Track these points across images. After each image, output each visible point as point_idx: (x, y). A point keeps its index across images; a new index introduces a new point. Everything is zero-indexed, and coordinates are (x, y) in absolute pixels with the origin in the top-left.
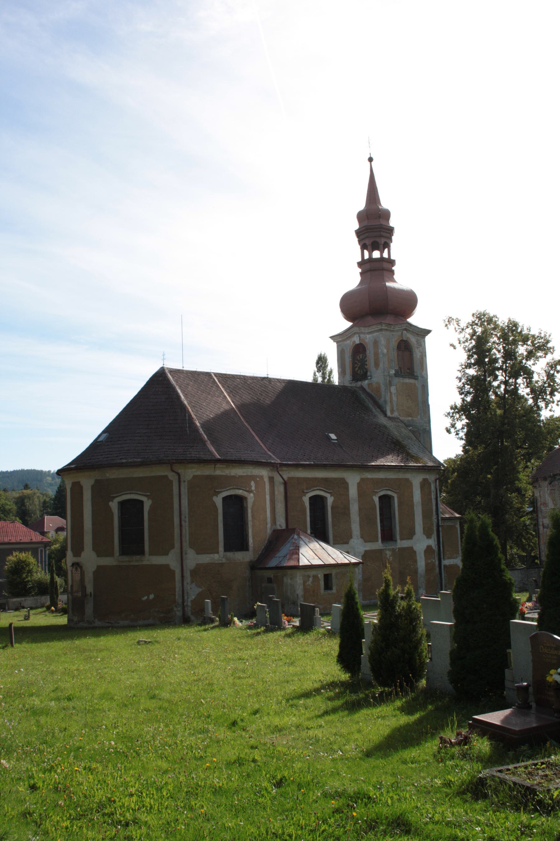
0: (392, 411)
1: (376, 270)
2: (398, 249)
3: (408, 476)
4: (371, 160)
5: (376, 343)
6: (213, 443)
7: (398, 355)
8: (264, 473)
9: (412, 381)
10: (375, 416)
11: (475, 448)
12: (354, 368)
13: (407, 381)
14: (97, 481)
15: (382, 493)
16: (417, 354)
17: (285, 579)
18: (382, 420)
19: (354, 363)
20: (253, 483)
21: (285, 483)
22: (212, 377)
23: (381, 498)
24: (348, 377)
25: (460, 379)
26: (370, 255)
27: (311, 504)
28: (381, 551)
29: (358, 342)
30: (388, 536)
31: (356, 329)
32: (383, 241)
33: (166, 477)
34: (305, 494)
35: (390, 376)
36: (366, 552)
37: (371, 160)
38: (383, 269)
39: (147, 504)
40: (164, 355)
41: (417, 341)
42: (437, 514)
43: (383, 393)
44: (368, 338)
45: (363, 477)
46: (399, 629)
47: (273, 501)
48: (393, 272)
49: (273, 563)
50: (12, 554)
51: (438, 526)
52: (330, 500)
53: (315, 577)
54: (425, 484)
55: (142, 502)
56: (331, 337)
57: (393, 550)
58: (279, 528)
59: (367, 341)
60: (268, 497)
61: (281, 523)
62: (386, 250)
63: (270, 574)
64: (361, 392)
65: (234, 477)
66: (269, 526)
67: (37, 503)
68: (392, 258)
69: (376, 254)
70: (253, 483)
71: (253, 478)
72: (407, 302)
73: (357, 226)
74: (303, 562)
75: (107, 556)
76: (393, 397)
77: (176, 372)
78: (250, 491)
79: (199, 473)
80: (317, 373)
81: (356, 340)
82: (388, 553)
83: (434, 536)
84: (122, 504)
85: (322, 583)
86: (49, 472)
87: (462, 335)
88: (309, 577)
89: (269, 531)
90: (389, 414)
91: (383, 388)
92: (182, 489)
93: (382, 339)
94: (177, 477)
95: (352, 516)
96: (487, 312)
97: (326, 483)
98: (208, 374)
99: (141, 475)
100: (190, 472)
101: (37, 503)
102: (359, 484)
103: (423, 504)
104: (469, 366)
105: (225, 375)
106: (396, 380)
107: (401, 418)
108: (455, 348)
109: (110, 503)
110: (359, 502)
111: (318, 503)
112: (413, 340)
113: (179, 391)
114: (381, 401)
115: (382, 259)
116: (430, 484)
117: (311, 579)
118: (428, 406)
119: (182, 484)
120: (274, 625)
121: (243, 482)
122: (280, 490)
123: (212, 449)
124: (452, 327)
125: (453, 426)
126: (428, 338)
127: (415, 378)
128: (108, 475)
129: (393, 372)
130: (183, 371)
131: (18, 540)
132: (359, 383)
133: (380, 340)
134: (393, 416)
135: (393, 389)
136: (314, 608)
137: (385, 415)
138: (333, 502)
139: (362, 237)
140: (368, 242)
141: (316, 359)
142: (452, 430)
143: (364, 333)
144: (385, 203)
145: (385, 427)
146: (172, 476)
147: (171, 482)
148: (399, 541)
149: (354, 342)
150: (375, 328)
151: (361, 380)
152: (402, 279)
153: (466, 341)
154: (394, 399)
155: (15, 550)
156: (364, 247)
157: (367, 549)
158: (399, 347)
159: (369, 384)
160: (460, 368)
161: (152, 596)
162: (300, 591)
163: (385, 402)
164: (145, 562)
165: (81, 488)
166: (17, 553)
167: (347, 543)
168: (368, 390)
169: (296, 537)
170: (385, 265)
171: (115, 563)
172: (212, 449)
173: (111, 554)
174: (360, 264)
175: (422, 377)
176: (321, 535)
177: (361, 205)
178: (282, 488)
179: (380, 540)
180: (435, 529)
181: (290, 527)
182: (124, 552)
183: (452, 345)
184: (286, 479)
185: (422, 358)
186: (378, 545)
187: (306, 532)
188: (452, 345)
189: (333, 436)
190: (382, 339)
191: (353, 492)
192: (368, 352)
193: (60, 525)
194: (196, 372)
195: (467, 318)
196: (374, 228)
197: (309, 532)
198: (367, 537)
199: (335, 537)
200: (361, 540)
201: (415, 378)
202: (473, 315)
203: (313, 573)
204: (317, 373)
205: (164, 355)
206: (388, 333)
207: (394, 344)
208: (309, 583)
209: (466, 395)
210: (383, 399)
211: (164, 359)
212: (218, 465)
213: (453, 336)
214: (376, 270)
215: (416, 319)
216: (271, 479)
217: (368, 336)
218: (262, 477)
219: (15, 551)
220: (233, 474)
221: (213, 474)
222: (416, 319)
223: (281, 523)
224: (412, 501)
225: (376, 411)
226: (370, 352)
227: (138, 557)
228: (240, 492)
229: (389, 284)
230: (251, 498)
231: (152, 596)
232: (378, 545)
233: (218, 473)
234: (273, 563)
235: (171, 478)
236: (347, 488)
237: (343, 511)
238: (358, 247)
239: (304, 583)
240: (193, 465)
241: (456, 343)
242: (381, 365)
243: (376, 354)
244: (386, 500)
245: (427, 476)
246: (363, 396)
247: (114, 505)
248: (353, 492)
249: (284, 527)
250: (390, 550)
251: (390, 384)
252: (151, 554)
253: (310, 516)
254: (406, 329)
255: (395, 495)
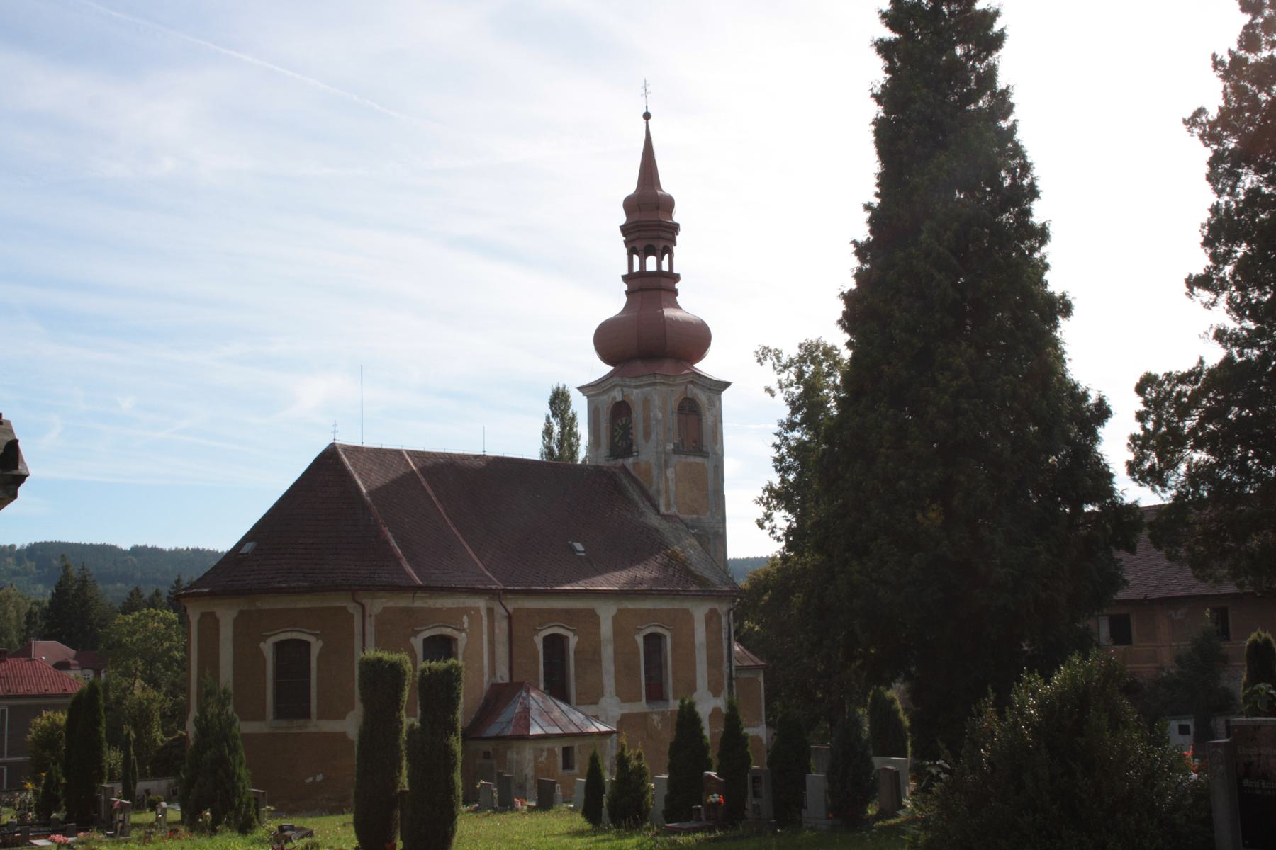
0: (668, 506)
1: (650, 290)
2: (686, 257)
3: (688, 605)
4: (647, 116)
5: (646, 402)
6: (410, 561)
7: (679, 420)
8: (481, 603)
9: (699, 460)
10: (642, 513)
11: (800, 554)
12: (612, 437)
13: (692, 459)
14: (242, 613)
15: (648, 631)
16: (708, 419)
17: (509, 755)
18: (653, 520)
19: (613, 430)
20: (465, 618)
21: (510, 617)
22: (404, 458)
23: (647, 638)
24: (604, 450)
25: (778, 447)
26: (642, 264)
27: (545, 647)
28: (644, 716)
29: (619, 399)
30: (656, 693)
31: (617, 380)
32: (662, 244)
33: (345, 608)
34: (536, 632)
35: (666, 453)
36: (624, 717)
37: (647, 116)
38: (660, 289)
39: (316, 647)
40: (335, 425)
41: (709, 399)
42: (730, 661)
43: (655, 479)
44: (635, 395)
45: (622, 607)
46: (630, 780)
47: (492, 643)
48: (675, 292)
49: (492, 731)
50: (41, 716)
51: (731, 678)
52: (573, 641)
53: (551, 751)
54: (712, 617)
55: (308, 644)
56: (580, 388)
57: (663, 714)
58: (500, 681)
59: (633, 398)
60: (485, 637)
61: (503, 675)
62: (666, 256)
63: (488, 747)
64: (622, 476)
65: (440, 610)
66: (486, 678)
67: (13, 615)
68: (675, 271)
69: (651, 264)
70: (465, 618)
71: (466, 611)
72: (696, 339)
73: (623, 219)
74: (531, 733)
75: (254, 719)
76: (669, 484)
77: (353, 451)
78: (461, 630)
79: (391, 604)
80: (552, 420)
81: (617, 395)
82: (655, 717)
83: (725, 693)
84: (279, 646)
85: (560, 759)
86: (12, 547)
87: (784, 376)
88: (542, 750)
89: (486, 686)
90: (663, 510)
91: (655, 472)
92: (367, 626)
93: (656, 397)
94: (360, 610)
95: (604, 664)
96: (823, 340)
97: (569, 617)
98: (398, 453)
99: (308, 605)
100: (378, 605)
101: (13, 615)
102: (615, 619)
103: (709, 648)
104: (791, 426)
105: (423, 453)
106: (675, 459)
107: (682, 516)
108: (773, 396)
109: (262, 645)
110: (615, 642)
111: (555, 645)
112: (702, 397)
113: (359, 482)
114: (652, 491)
115: (659, 273)
116: (719, 617)
117: (545, 754)
118: (723, 496)
119: (368, 619)
120: (505, 805)
121: (452, 617)
122: (502, 626)
123: (409, 569)
124: (769, 363)
125: (768, 517)
126: (725, 395)
127: (704, 455)
128: (258, 604)
129: (670, 447)
130: (362, 448)
131: (42, 690)
132: (620, 461)
133: (655, 400)
134: (669, 512)
135: (670, 473)
136: (554, 783)
137: (658, 512)
138: (578, 643)
139: (631, 237)
140: (640, 245)
141: (549, 394)
142: (767, 524)
143: (629, 387)
144: (668, 185)
145: (657, 530)
146: (352, 607)
147: (352, 616)
148: (671, 701)
149: (614, 398)
150: (645, 380)
151: (623, 457)
152: (691, 302)
153: (791, 385)
154: (672, 487)
155: (46, 707)
156: (631, 252)
157: (626, 711)
158: (681, 409)
159: (636, 465)
160: (778, 429)
161: (320, 778)
162: (529, 771)
163: (658, 491)
164: (312, 729)
165: (217, 621)
166: (51, 713)
167: (597, 703)
168: (633, 473)
169: (524, 694)
170: (664, 282)
171: (266, 731)
172: (409, 569)
173: (261, 717)
174: (626, 278)
175: (715, 453)
176: (557, 689)
177: (630, 186)
178: (505, 624)
179: (644, 700)
180: (726, 683)
181: (515, 680)
182: (280, 713)
183: (768, 390)
184: (511, 611)
185: (716, 425)
186: (641, 706)
187: (537, 688)
188: (768, 390)
189: (579, 546)
190: (656, 397)
191: (606, 629)
192: (634, 415)
193: (61, 658)
194: (380, 449)
195: (791, 351)
196: (649, 222)
197: (542, 686)
198: (625, 695)
199: (578, 694)
200: (616, 700)
201: (704, 455)
202: (800, 346)
203: (546, 745)
204: (552, 420)
205: (335, 425)
206: (664, 388)
207: (673, 404)
208: (542, 759)
209: (785, 472)
210: (654, 488)
211: (335, 432)
212: (419, 594)
213: (769, 376)
214: (650, 290)
215: (707, 366)
216: (490, 611)
217: (635, 391)
218: (477, 610)
219: (46, 710)
220: (438, 606)
221: (411, 605)
222: (707, 366)
223: (503, 675)
224: (693, 643)
225: (644, 506)
226: (637, 415)
227: (301, 722)
228: (448, 631)
229: (669, 312)
230: (462, 638)
231: (320, 778)
232: (641, 706)
233: (418, 604)
234: (492, 731)
235: (351, 611)
236: (597, 624)
237: (591, 657)
238: (623, 251)
239: (536, 759)
240: (381, 594)
241: (775, 387)
242: (653, 437)
243: (647, 420)
244: (654, 642)
245: (716, 606)
246: (625, 482)
247: (267, 648)
248: (606, 629)
249: (506, 680)
250: (657, 713)
251: (666, 465)
252: (319, 718)
253: (545, 665)
254: (692, 382)
255: (667, 634)
